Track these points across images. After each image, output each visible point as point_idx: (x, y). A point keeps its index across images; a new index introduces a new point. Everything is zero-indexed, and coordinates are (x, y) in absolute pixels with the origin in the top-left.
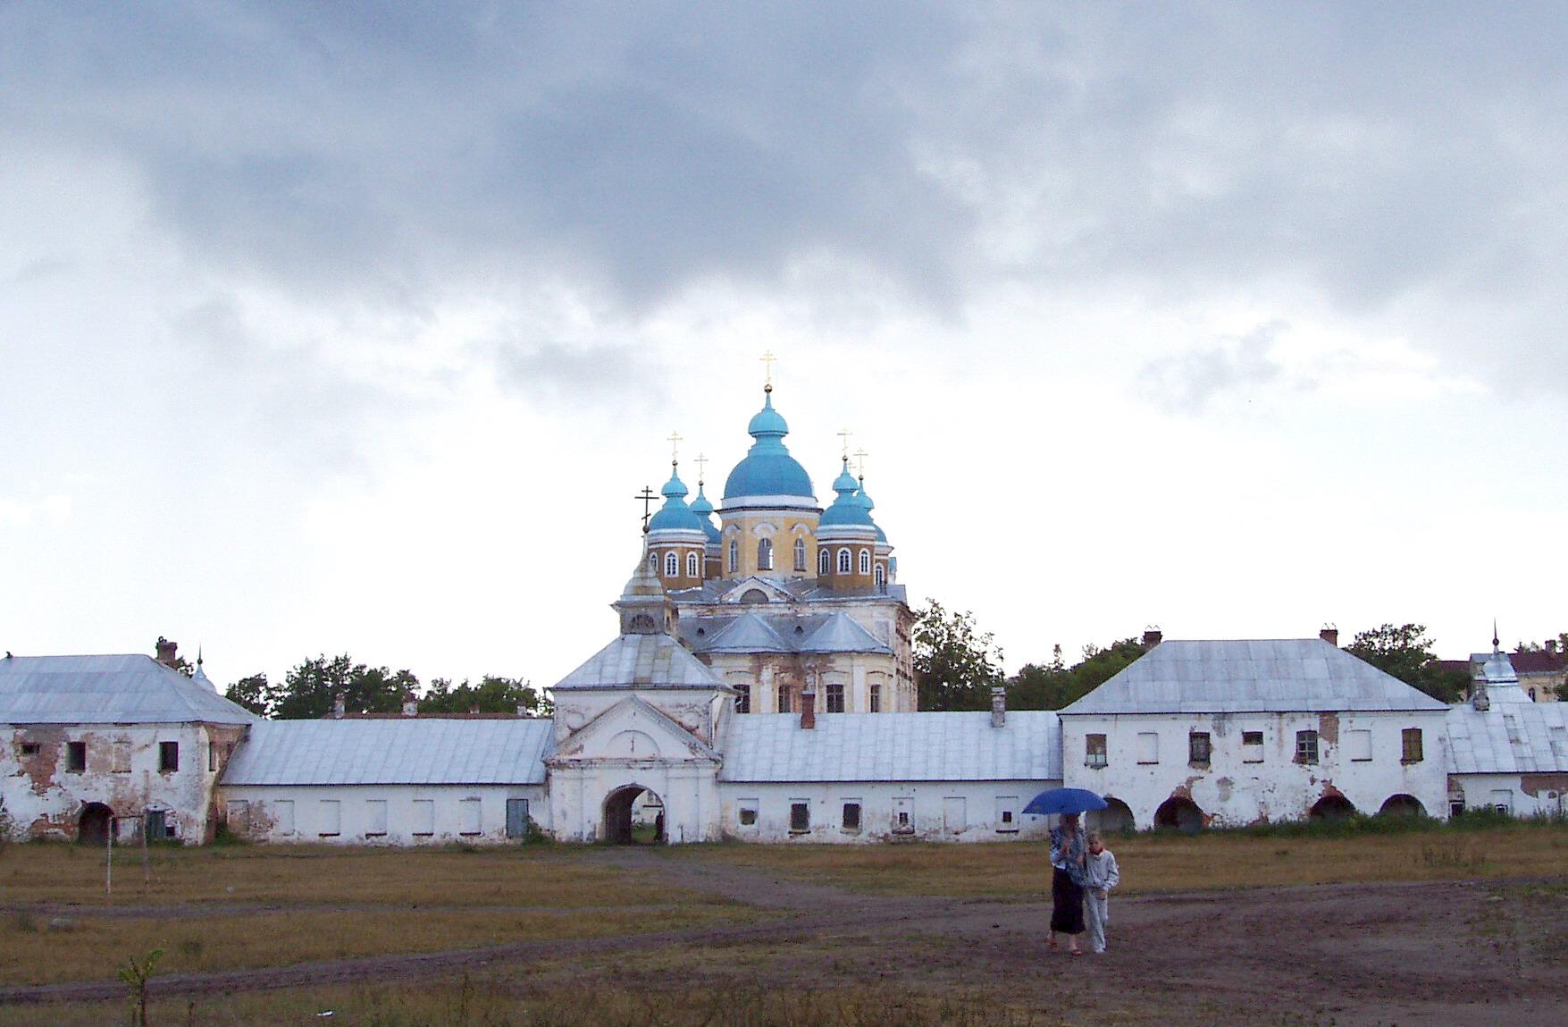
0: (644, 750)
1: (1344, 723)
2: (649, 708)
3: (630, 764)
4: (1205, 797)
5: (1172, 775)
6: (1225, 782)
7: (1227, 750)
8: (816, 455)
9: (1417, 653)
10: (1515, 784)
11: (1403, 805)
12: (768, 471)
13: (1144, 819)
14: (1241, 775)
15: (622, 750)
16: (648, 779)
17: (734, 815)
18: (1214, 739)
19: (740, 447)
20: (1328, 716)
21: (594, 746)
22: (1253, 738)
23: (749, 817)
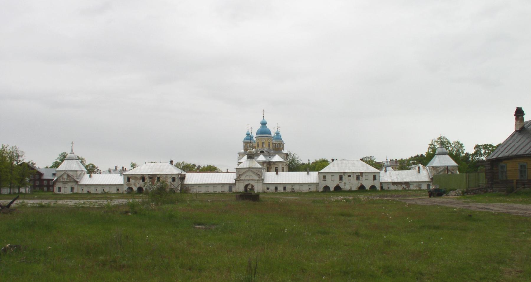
0: (251, 178)
1: (364, 174)
2: (252, 171)
3: (249, 180)
4: (342, 186)
5: (337, 182)
6: (345, 183)
7: (345, 178)
8: (271, 127)
9: (373, 161)
10: (391, 184)
11: (373, 188)
12: (264, 131)
13: (332, 189)
14: (347, 182)
15: (247, 178)
16: (252, 183)
17: (266, 188)
18: (343, 176)
19: (259, 126)
20: (362, 173)
21: (243, 178)
22: (349, 176)
23: (268, 189)
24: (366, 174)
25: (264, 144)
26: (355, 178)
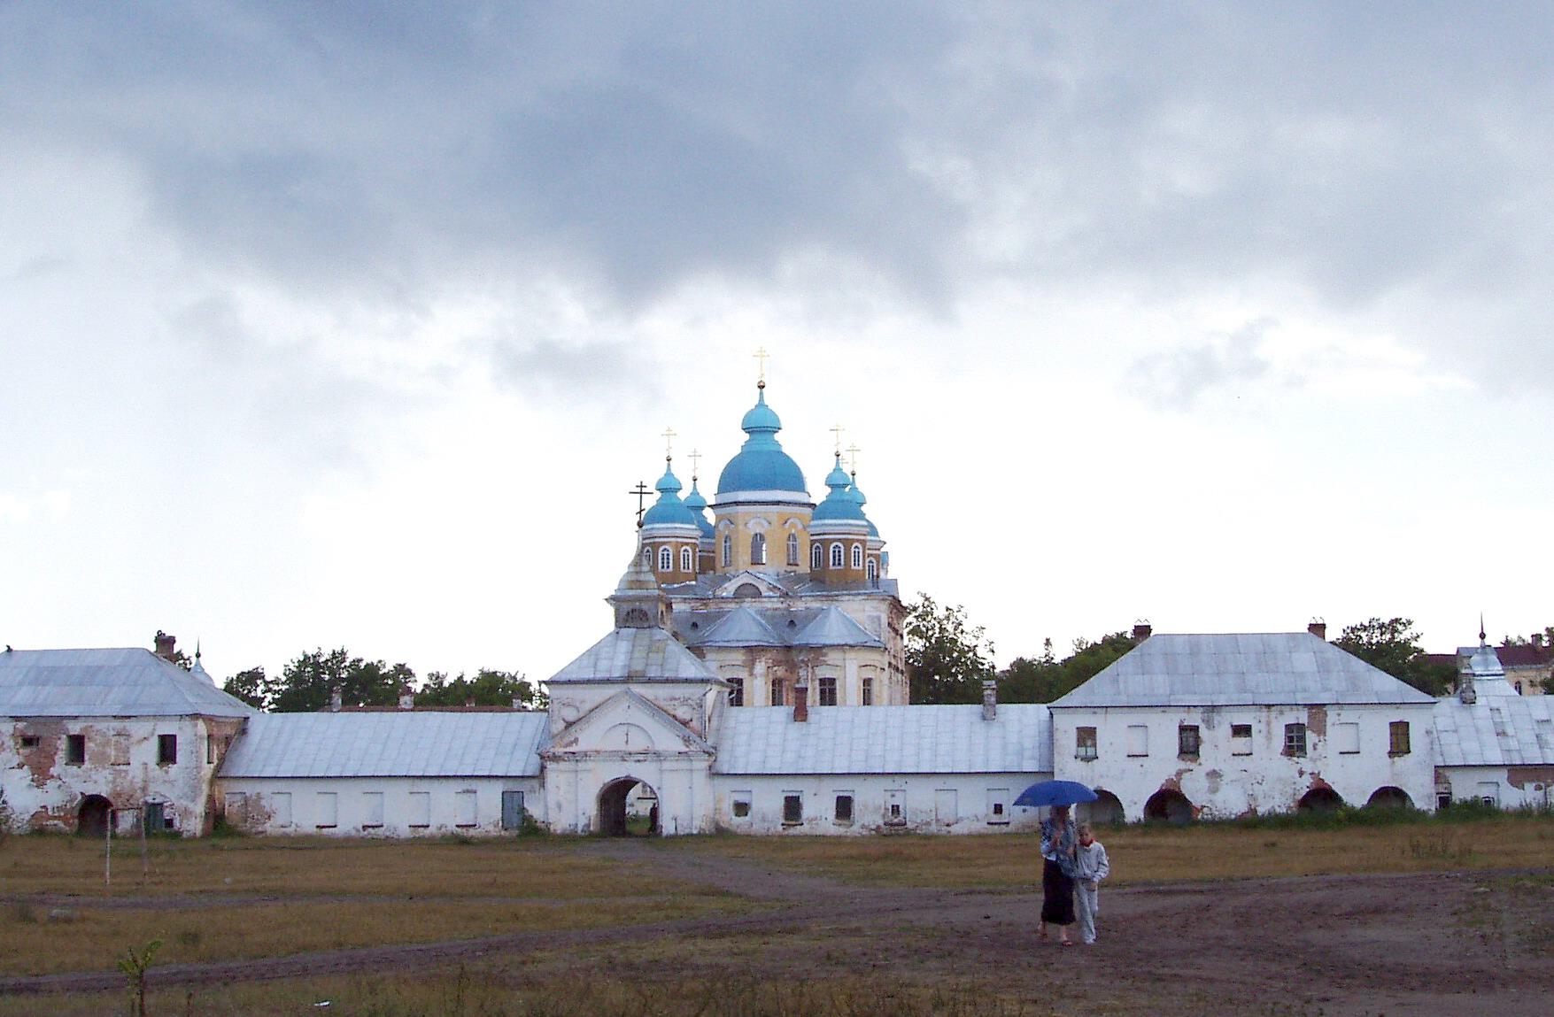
0: (638, 743)
1: (1332, 716)
3: (624, 756)
4: (1195, 789)
5: (1162, 767)
6: (1214, 775)
7: (1217, 743)
8: (809, 451)
9: (1405, 647)
10: (1502, 776)
11: (1390, 797)
12: (761, 466)
13: (1134, 811)
14: (1230, 768)
15: (616, 742)
16: (643, 771)
17: (727, 807)
19: (733, 442)
20: (1317, 709)
22: (1242, 731)
23: (742, 809)
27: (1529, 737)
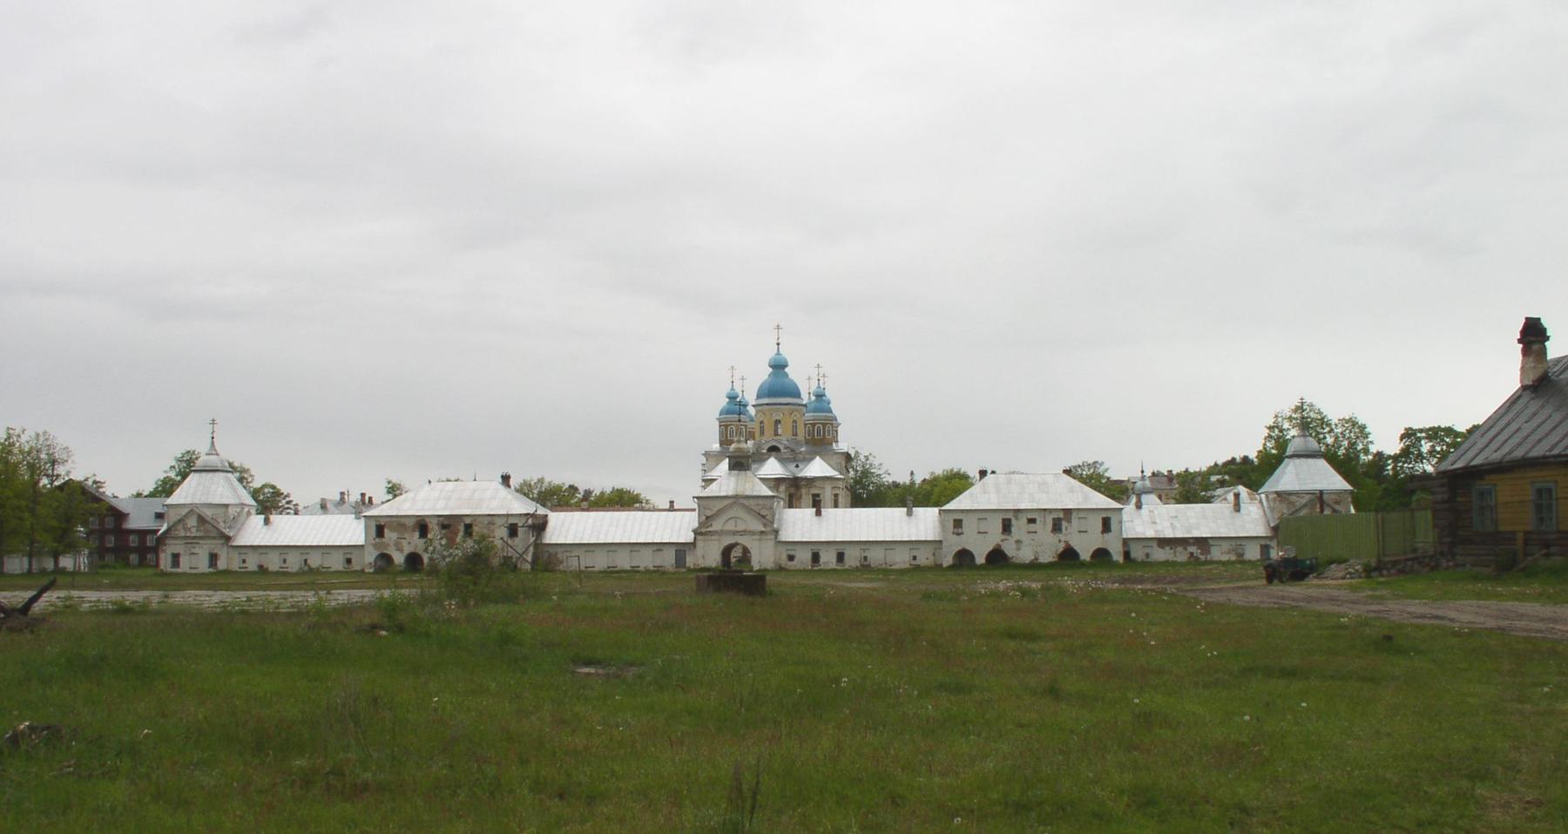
0: (741, 527)
1: (1074, 515)
3: (735, 533)
4: (1009, 549)
5: (994, 537)
6: (1018, 542)
7: (1019, 527)
8: (801, 376)
9: (1100, 476)
10: (1155, 544)
11: (1101, 555)
12: (779, 387)
13: (980, 559)
14: (1026, 538)
15: (730, 526)
16: (745, 541)
17: (784, 557)
18: (1014, 522)
19: (763, 373)
20: (1068, 512)
22: (1032, 521)
23: (791, 558)
24: (1082, 515)
25: (779, 427)
26: (1050, 526)
27: (1167, 524)
